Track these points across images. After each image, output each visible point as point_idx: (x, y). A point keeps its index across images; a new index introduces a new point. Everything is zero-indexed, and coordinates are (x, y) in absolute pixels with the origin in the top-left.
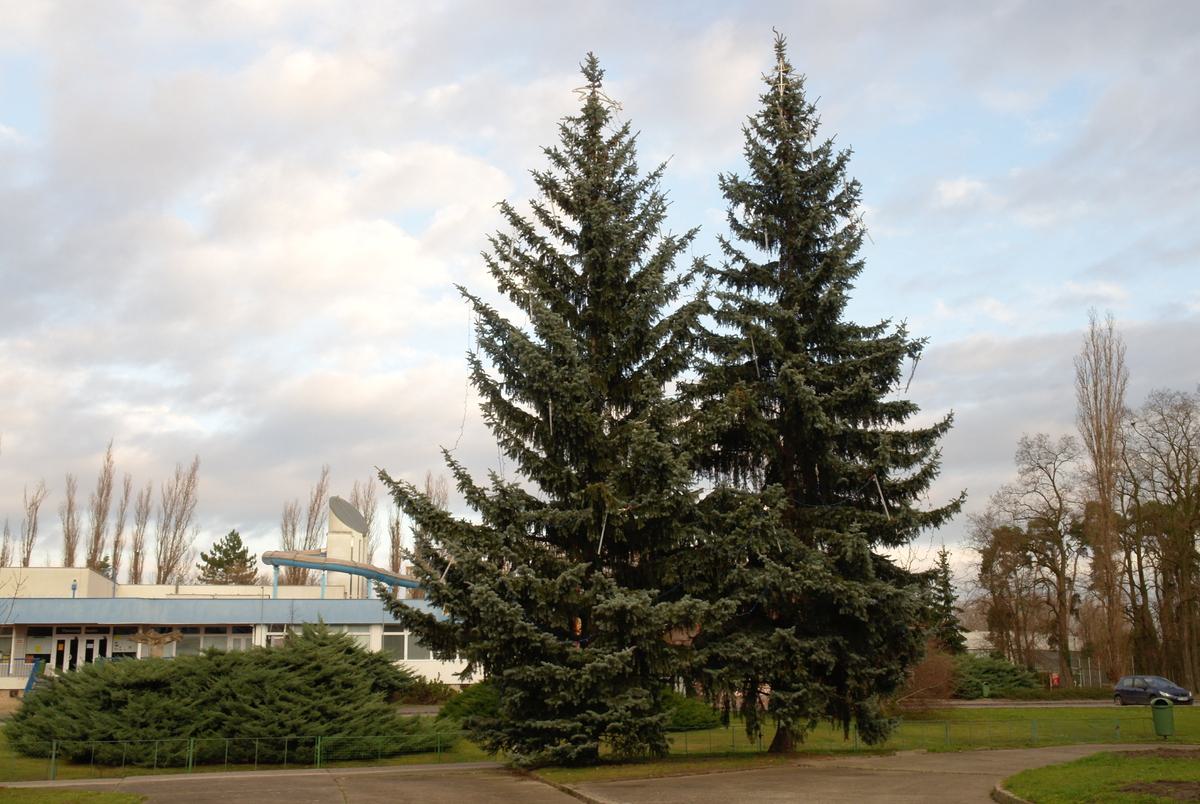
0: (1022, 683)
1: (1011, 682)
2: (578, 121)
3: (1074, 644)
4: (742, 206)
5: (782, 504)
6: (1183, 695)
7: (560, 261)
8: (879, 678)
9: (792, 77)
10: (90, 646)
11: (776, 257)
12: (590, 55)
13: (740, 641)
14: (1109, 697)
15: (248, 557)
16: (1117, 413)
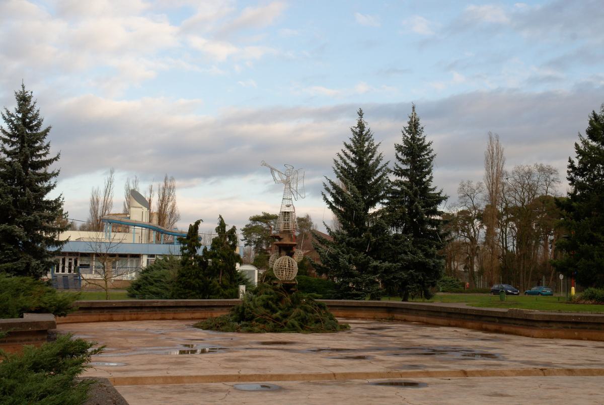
0: (455, 286)
1: (451, 286)
2: (356, 128)
3: (476, 269)
4: (401, 153)
5: (413, 239)
6: (516, 292)
7: (353, 169)
8: (432, 283)
9: (417, 117)
10: (70, 261)
11: (409, 167)
12: (360, 109)
13: (401, 273)
14: (489, 293)
15: (64, 212)
16: (500, 174)
